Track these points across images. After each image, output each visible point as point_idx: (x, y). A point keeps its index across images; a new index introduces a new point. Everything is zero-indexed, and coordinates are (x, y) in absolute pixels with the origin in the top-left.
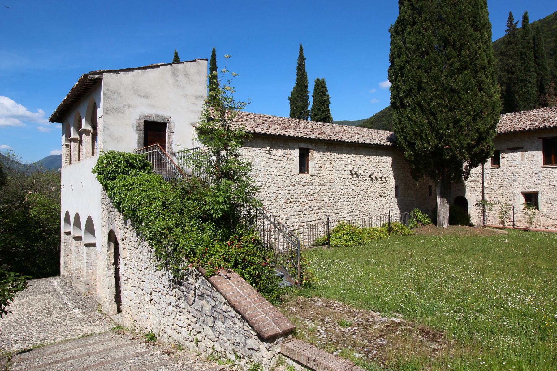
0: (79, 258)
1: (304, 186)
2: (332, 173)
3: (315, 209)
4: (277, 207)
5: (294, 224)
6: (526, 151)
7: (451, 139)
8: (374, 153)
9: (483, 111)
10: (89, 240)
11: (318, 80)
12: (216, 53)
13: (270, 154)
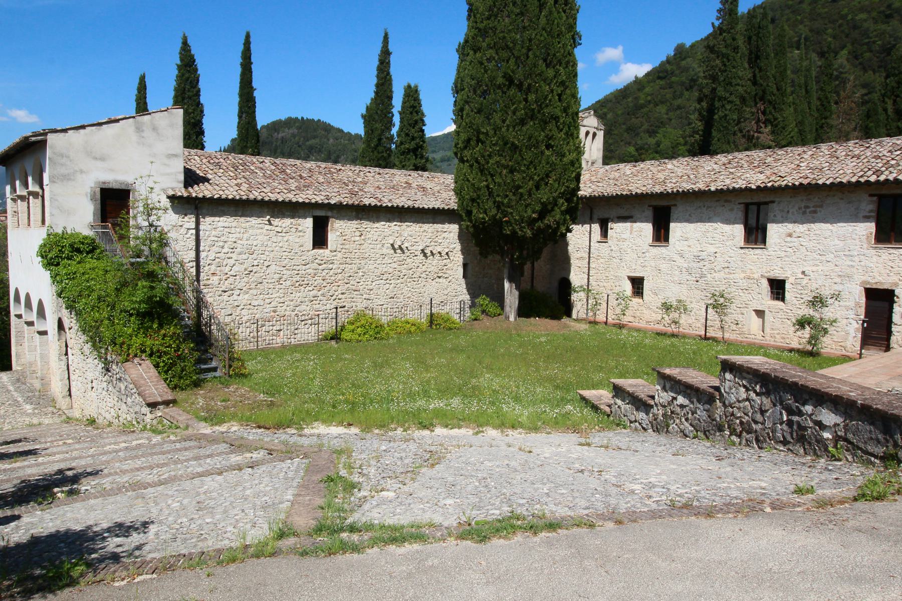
0: (32, 349)
1: (320, 265)
2: (363, 247)
3: (336, 293)
4: (281, 291)
5: (304, 313)
6: (635, 222)
7: (510, 210)
8: (431, 220)
9: (550, 175)
10: (40, 327)
11: (409, 86)
12: (251, 40)
13: (270, 224)
